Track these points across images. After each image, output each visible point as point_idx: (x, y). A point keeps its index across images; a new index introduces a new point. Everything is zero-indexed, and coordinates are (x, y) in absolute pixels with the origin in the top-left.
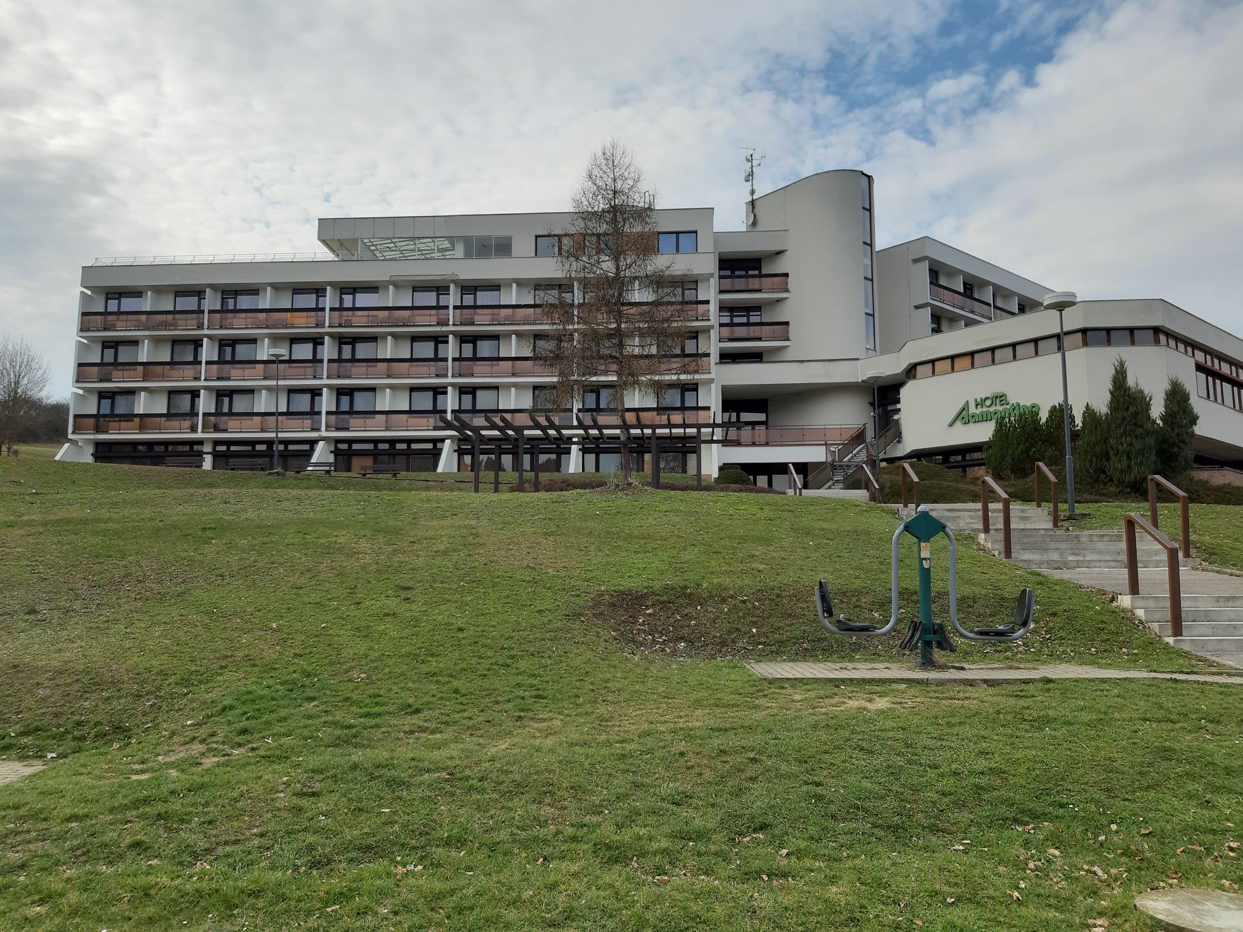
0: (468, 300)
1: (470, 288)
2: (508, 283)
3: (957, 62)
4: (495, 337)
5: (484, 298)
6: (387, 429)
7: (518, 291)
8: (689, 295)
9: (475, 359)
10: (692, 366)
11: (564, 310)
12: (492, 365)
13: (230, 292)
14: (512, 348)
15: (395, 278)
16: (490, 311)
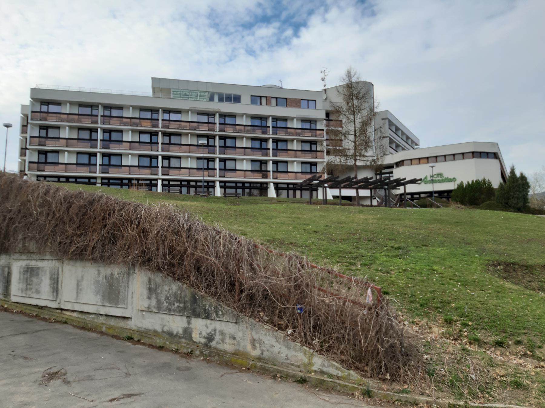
0: (107, 113)
1: (223, 115)
2: (128, 107)
3: (265, 20)
4: (180, 135)
5: (115, 113)
6: (66, 172)
7: (70, 107)
8: (313, 127)
9: (47, 137)
10: (314, 155)
11: (264, 128)
12: (305, 154)
13: (110, 107)
14: (295, 146)
15: (192, 109)
16: (179, 123)
